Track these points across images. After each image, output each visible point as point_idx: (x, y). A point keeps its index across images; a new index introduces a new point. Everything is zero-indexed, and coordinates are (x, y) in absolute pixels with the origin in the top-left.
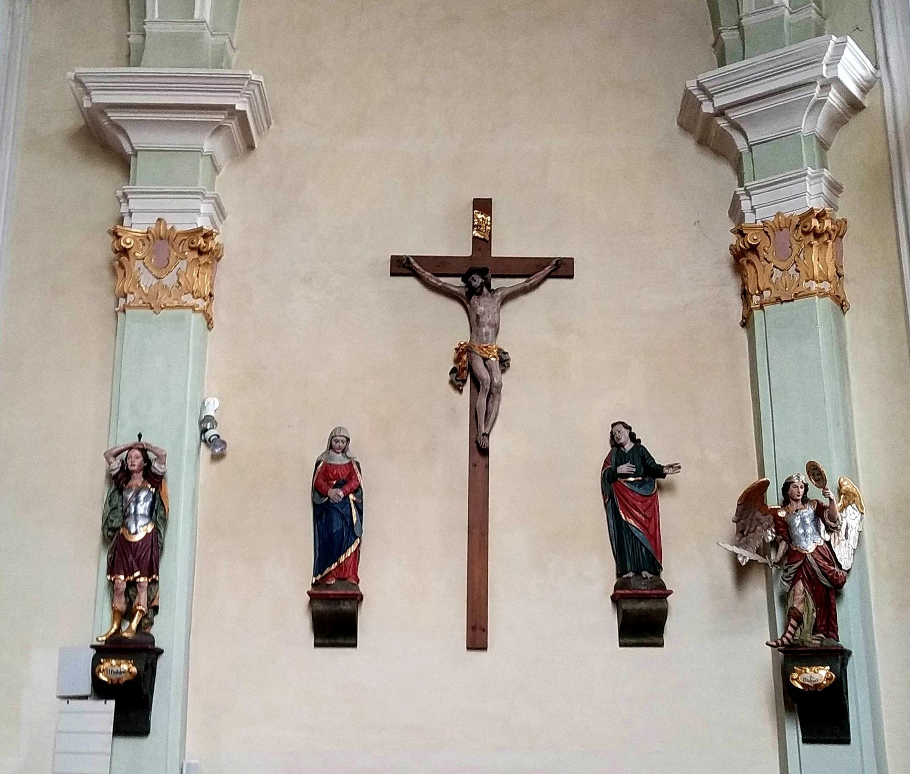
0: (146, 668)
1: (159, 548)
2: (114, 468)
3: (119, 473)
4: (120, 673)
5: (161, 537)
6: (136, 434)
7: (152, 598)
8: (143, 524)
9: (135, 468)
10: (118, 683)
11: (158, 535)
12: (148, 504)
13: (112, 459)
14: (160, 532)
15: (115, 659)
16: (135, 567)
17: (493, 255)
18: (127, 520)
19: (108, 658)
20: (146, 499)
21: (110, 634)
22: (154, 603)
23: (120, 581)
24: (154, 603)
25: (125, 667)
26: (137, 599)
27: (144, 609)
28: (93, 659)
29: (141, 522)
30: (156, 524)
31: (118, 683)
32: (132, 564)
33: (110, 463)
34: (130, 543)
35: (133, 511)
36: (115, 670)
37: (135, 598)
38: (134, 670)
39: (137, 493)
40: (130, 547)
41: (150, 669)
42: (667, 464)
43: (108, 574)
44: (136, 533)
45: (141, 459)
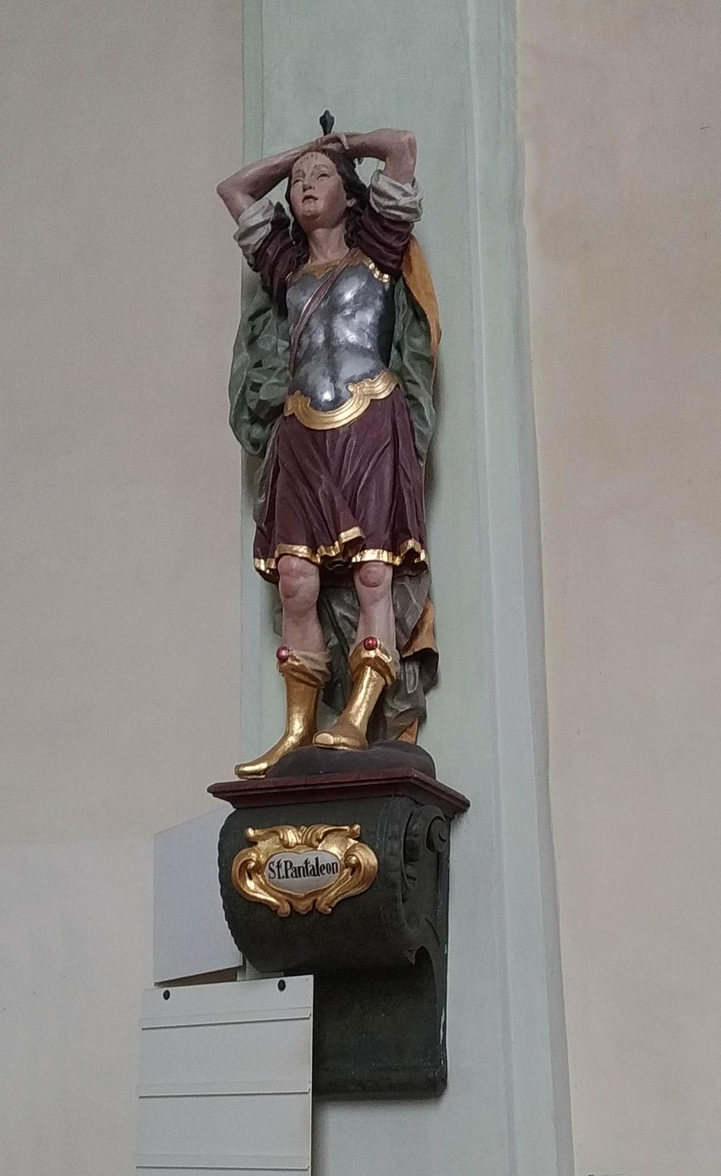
0: (410, 854)
1: (419, 456)
2: (252, 223)
3: (268, 240)
4: (318, 870)
5: (423, 418)
6: (317, 116)
7: (411, 622)
8: (358, 372)
9: (319, 206)
10: (313, 910)
11: (414, 416)
12: (368, 317)
13: (242, 200)
14: (418, 406)
15: (297, 827)
16: (344, 514)
17: (311, 978)
18: (303, 370)
19: (271, 825)
20: (360, 302)
21: (280, 752)
22: (422, 643)
23: (295, 563)
24: (422, 643)
25: (334, 849)
26: (361, 627)
27: (387, 660)
28: (224, 833)
29: (351, 367)
30: (401, 377)
31: (313, 910)
32: (332, 503)
33: (236, 214)
34: (319, 438)
35: (320, 339)
36: (298, 862)
37: (355, 627)
38: (367, 857)
39: (333, 281)
40: (321, 449)
41: (426, 857)
42: (468, 798)
43: (256, 556)
44: (337, 403)
45: (334, 180)
